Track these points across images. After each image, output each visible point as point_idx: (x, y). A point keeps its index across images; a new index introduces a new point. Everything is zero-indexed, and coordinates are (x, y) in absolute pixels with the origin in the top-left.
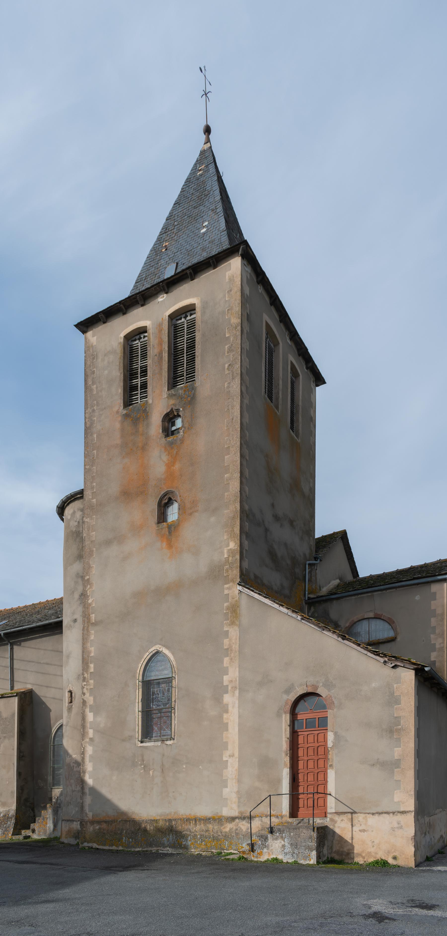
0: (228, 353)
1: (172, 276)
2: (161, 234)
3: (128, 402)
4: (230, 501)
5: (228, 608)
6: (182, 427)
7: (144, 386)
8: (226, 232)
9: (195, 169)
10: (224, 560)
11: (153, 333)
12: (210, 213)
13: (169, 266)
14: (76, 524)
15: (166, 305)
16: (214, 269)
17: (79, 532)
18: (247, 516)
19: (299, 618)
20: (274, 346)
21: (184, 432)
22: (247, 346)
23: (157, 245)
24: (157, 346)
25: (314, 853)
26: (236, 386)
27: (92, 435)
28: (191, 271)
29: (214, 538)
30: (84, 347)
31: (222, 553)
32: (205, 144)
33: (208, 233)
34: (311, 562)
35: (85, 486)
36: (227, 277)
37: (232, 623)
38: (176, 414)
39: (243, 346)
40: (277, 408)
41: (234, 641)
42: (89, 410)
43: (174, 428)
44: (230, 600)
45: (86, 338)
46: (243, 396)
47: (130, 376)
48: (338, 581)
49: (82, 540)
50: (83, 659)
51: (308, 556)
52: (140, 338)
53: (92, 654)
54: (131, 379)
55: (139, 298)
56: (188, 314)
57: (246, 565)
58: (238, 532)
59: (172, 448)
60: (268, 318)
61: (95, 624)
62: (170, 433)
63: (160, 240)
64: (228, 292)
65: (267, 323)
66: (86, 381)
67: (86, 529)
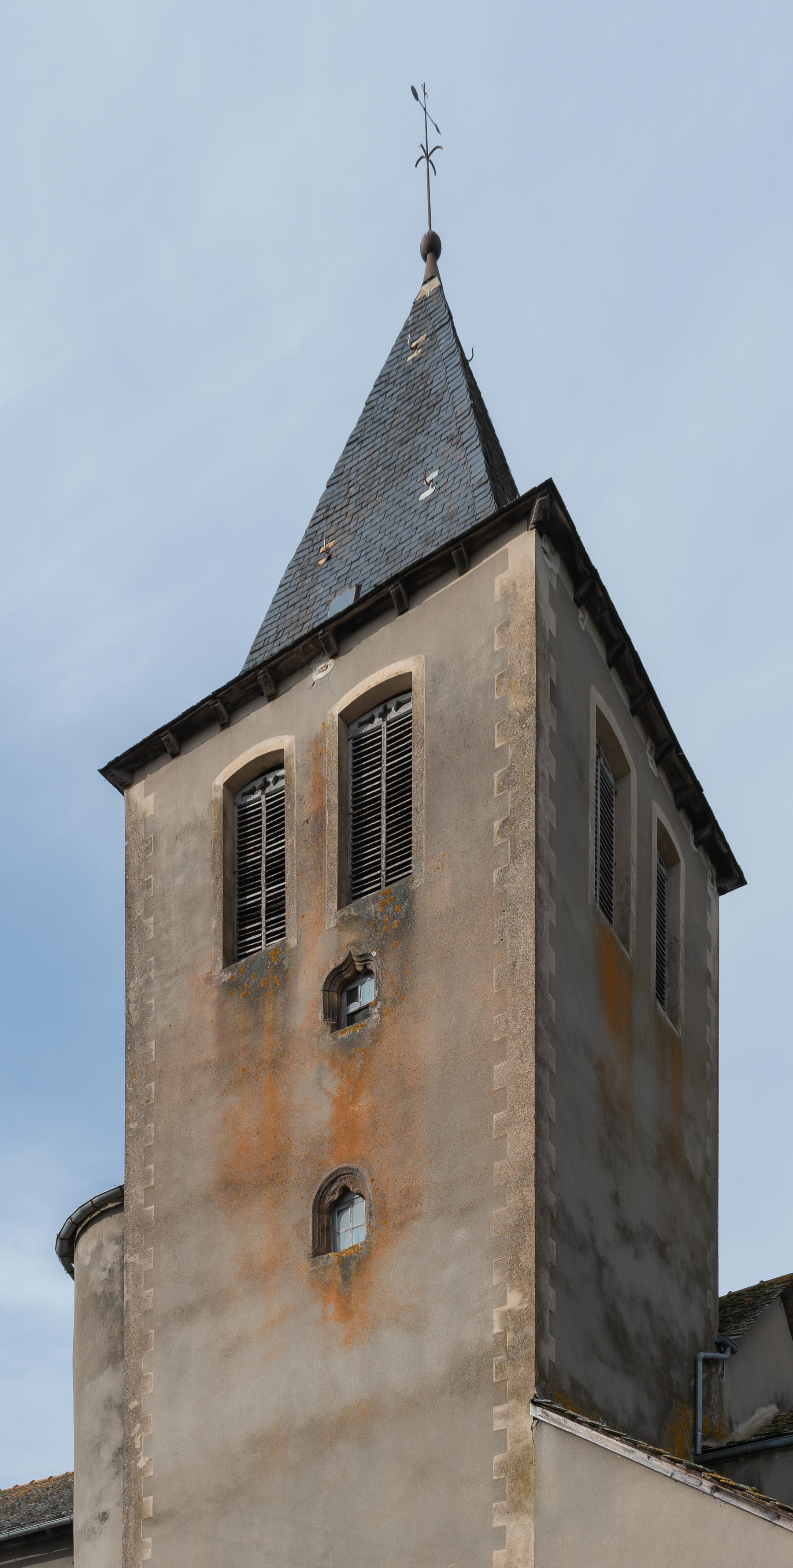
0: (500, 789)
1: (350, 608)
2: (315, 522)
3: (236, 947)
4: (508, 1182)
5: (503, 1468)
6: (377, 999)
7: (277, 906)
8: (488, 486)
9: (401, 346)
10: (491, 1339)
11: (298, 766)
12: (443, 446)
13: (338, 597)
14: (105, 1275)
15: (333, 687)
16: (461, 573)
17: (111, 1294)
18: (554, 1223)
19: (706, 1486)
20: (616, 779)
21: (381, 1013)
22: (551, 769)
23: (306, 552)
24: (312, 802)
26: (522, 877)
27: (144, 1043)
28: (400, 586)
29: (467, 1283)
30: (123, 824)
31: (488, 1322)
32: (425, 283)
33: (440, 497)
34: (709, 1354)
35: (127, 1176)
36: (497, 590)
37: (516, 1508)
38: (359, 969)
39: (541, 768)
40: (625, 940)
41: (519, 1555)
42: (137, 981)
43: (354, 1007)
44: (509, 1447)
45: (128, 802)
46: (542, 902)
47: (240, 884)
49: (121, 1313)
51: (700, 1337)
52: (266, 784)
54: (242, 893)
55: (266, 678)
56: (392, 705)
57: (550, 1352)
58: (531, 1264)
59: (351, 1057)
60: (603, 700)
61: (154, 1521)
62: (344, 1019)
63: (311, 538)
64: (500, 629)
65: (598, 711)
66: (128, 908)
67: (131, 1283)
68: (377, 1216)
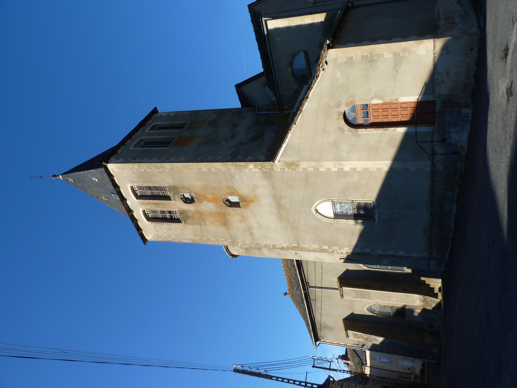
3: (178, 221)
5: (289, 169)
7: (170, 212)
15: (132, 201)
19: (294, 126)
25: (464, 110)
29: (246, 176)
31: (256, 172)
37: (298, 166)
40: (173, 138)
48: (266, 88)
50: (320, 252)
53: (317, 246)
57: (262, 158)
58: (244, 163)
60: (131, 146)
68: (232, 194)
